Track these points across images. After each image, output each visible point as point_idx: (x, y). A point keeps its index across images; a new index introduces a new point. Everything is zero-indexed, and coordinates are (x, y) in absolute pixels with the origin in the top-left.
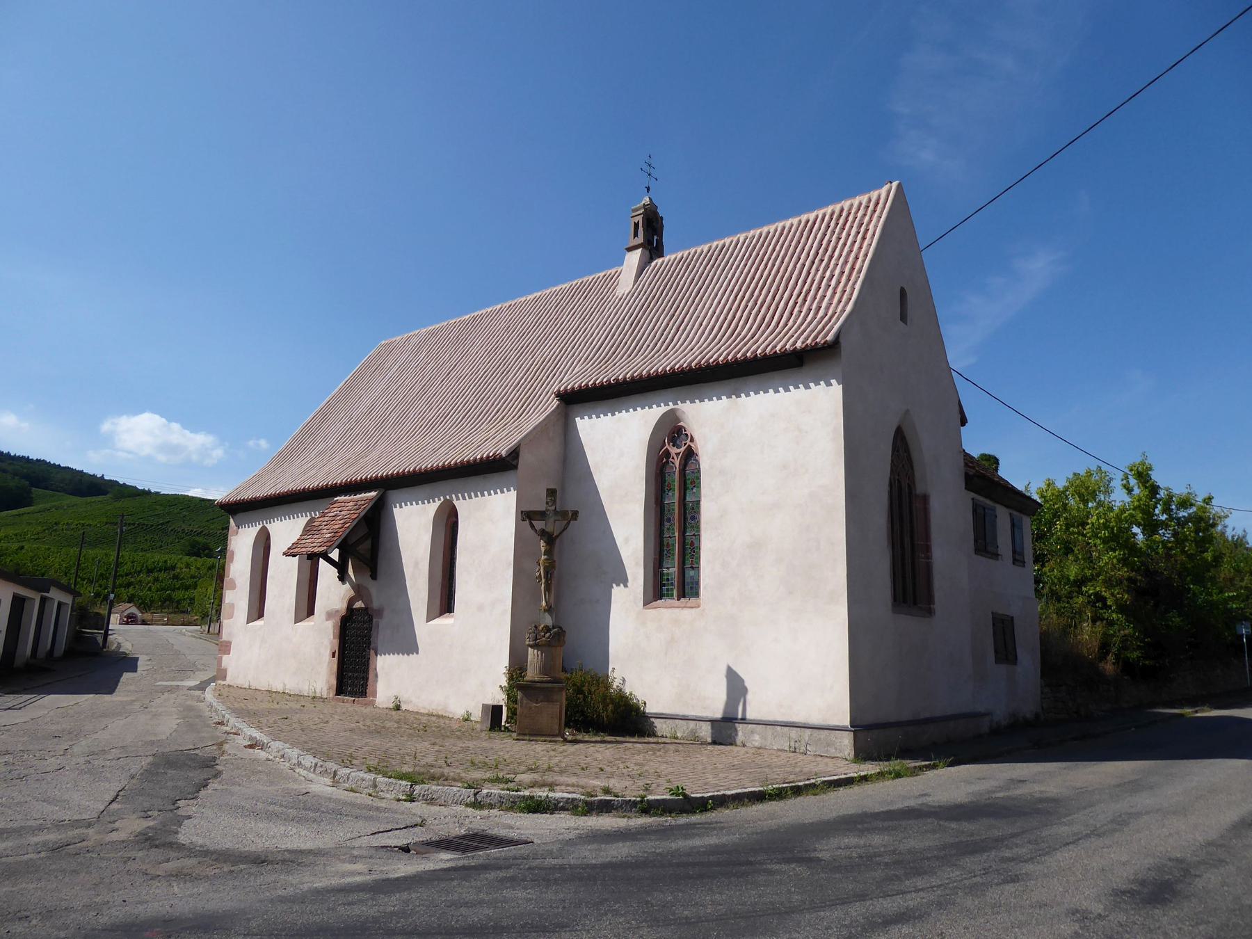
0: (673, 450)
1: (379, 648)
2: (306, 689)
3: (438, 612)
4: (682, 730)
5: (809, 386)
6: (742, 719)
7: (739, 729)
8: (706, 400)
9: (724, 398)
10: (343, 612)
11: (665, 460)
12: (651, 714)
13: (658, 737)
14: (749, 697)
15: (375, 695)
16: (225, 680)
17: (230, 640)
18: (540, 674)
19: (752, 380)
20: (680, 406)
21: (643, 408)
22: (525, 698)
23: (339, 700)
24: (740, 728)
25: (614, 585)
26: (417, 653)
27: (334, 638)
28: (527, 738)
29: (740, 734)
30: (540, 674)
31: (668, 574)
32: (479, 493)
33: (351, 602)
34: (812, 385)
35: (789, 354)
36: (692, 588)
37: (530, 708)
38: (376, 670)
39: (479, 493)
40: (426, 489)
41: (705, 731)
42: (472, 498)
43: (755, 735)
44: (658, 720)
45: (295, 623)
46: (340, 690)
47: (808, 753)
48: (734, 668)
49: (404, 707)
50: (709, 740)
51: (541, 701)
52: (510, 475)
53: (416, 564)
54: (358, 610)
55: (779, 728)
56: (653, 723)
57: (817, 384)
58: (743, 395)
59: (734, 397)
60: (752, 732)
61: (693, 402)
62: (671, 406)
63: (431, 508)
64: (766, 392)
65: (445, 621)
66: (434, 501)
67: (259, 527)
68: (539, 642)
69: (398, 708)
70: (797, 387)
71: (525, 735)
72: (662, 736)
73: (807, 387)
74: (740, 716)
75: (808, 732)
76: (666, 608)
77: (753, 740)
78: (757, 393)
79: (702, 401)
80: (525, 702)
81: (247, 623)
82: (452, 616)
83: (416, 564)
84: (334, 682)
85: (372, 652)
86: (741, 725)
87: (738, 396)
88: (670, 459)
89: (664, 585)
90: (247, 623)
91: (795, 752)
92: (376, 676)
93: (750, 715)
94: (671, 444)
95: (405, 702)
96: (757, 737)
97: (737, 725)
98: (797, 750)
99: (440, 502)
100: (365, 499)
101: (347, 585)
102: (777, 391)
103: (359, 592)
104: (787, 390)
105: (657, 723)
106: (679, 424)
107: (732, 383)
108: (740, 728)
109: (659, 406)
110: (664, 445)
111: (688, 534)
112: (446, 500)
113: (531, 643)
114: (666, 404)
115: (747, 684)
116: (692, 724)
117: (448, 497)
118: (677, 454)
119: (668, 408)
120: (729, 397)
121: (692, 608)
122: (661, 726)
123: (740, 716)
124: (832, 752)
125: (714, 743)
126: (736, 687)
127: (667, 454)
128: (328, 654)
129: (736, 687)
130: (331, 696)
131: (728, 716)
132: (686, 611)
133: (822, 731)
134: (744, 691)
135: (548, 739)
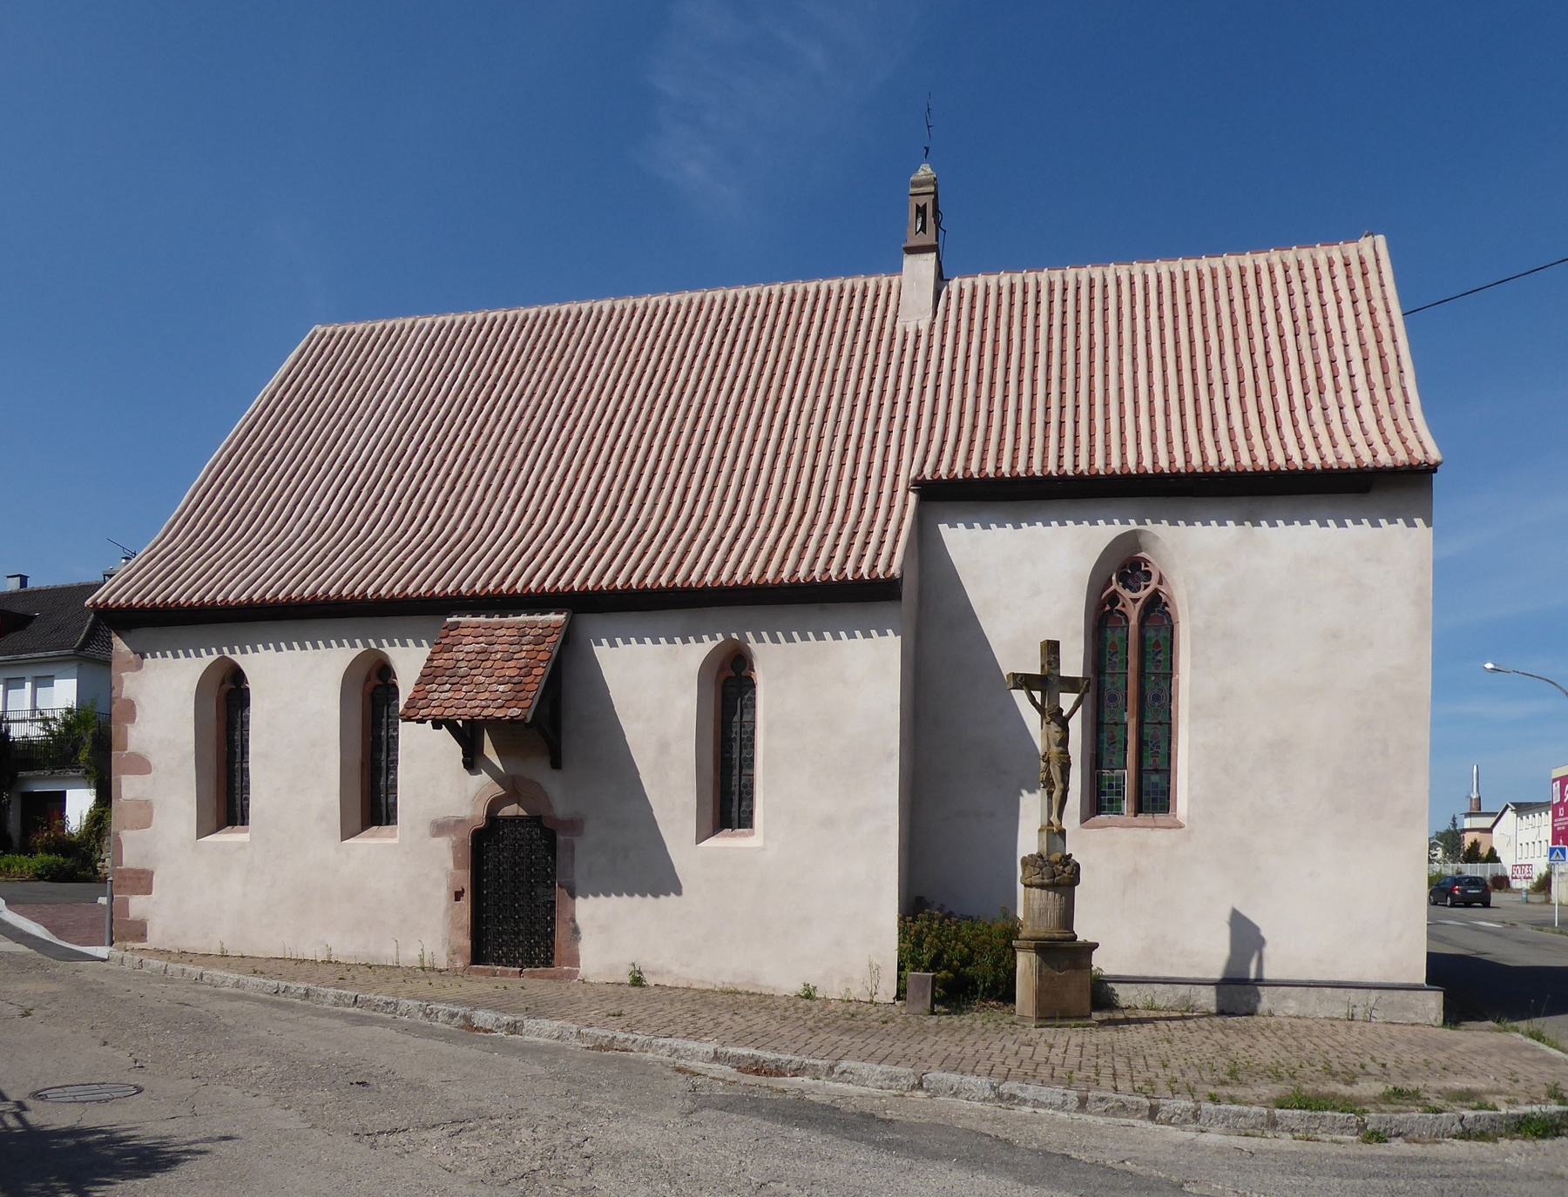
0: (1127, 594)
1: (579, 883)
2: (410, 956)
3: (214, 825)
4: (1165, 997)
5: (1379, 523)
6: (1256, 980)
7: (1262, 993)
8: (1198, 524)
9: (1230, 523)
10: (480, 822)
11: (1108, 608)
12: (1107, 976)
13: (1122, 1008)
14: (1267, 950)
15: (574, 960)
16: (146, 941)
17: (148, 867)
18: (1060, 928)
19: (1277, 502)
20: (1149, 526)
21: (1078, 522)
22: (1044, 964)
23: (477, 972)
24: (1264, 992)
25: (1024, 792)
26: (679, 892)
27: (457, 864)
28: (1058, 1023)
29: (1264, 999)
30: (1060, 928)
31: (1111, 779)
32: (236, 647)
33: (494, 805)
34: (1383, 522)
35: (1370, 472)
36: (1154, 800)
37: (1053, 979)
38: (574, 921)
39: (236, 647)
40: (678, 618)
41: (1207, 998)
42: (247, 653)
43: (1290, 1000)
44: (1121, 985)
45: (342, 841)
46: (479, 955)
47: (1373, 1020)
48: (1245, 912)
49: (650, 980)
50: (1213, 1009)
51: (1067, 968)
52: (885, 609)
53: (664, 747)
54: (512, 820)
55: (1328, 990)
56: (1113, 989)
57: (1392, 521)
58: (1264, 523)
59: (1248, 524)
60: (1285, 997)
61: (1173, 523)
62: (1133, 525)
63: (696, 652)
64: (1305, 522)
65: (726, 842)
66: (198, 655)
67: (207, 659)
68: (1059, 880)
69: (637, 981)
70: (1357, 522)
71: (1053, 1018)
72: (1128, 1007)
73: (1376, 524)
74: (1252, 975)
75: (1375, 993)
76: (1122, 827)
77: (1286, 1007)
78: (1289, 522)
79: (1190, 523)
80: (1044, 970)
81: (197, 839)
82: (247, 831)
83: (664, 747)
84: (466, 943)
85: (560, 893)
86: (1266, 988)
87: (1256, 524)
88: (1119, 607)
89: (1104, 793)
90: (197, 839)
91: (1352, 1020)
92: (576, 931)
93: (1269, 974)
94: (1121, 584)
95: (653, 973)
96: (1292, 1003)
97: (1260, 988)
98: (1356, 1018)
99: (714, 644)
100: (540, 625)
101: (484, 777)
102: (1323, 524)
103: (513, 787)
104: (1341, 524)
105: (1119, 989)
106: (1138, 555)
107: (1245, 503)
108: (1264, 992)
109: (1109, 522)
110: (1110, 582)
111: (1147, 721)
112: (728, 640)
113: (1046, 881)
114: (1124, 522)
115: (1264, 933)
116: (1183, 990)
117: (374, 646)
118: (1135, 601)
119: (1125, 529)
120: (1240, 523)
121: (1170, 828)
122: (1124, 994)
123: (1252, 975)
124: (1412, 1017)
125: (1221, 1012)
126: (1245, 936)
127: (1114, 598)
128: (442, 894)
129: (1245, 936)
130: (459, 964)
131: (1227, 977)
132: (1159, 833)
133: (1395, 992)
134: (1260, 943)
135: (1081, 1022)
